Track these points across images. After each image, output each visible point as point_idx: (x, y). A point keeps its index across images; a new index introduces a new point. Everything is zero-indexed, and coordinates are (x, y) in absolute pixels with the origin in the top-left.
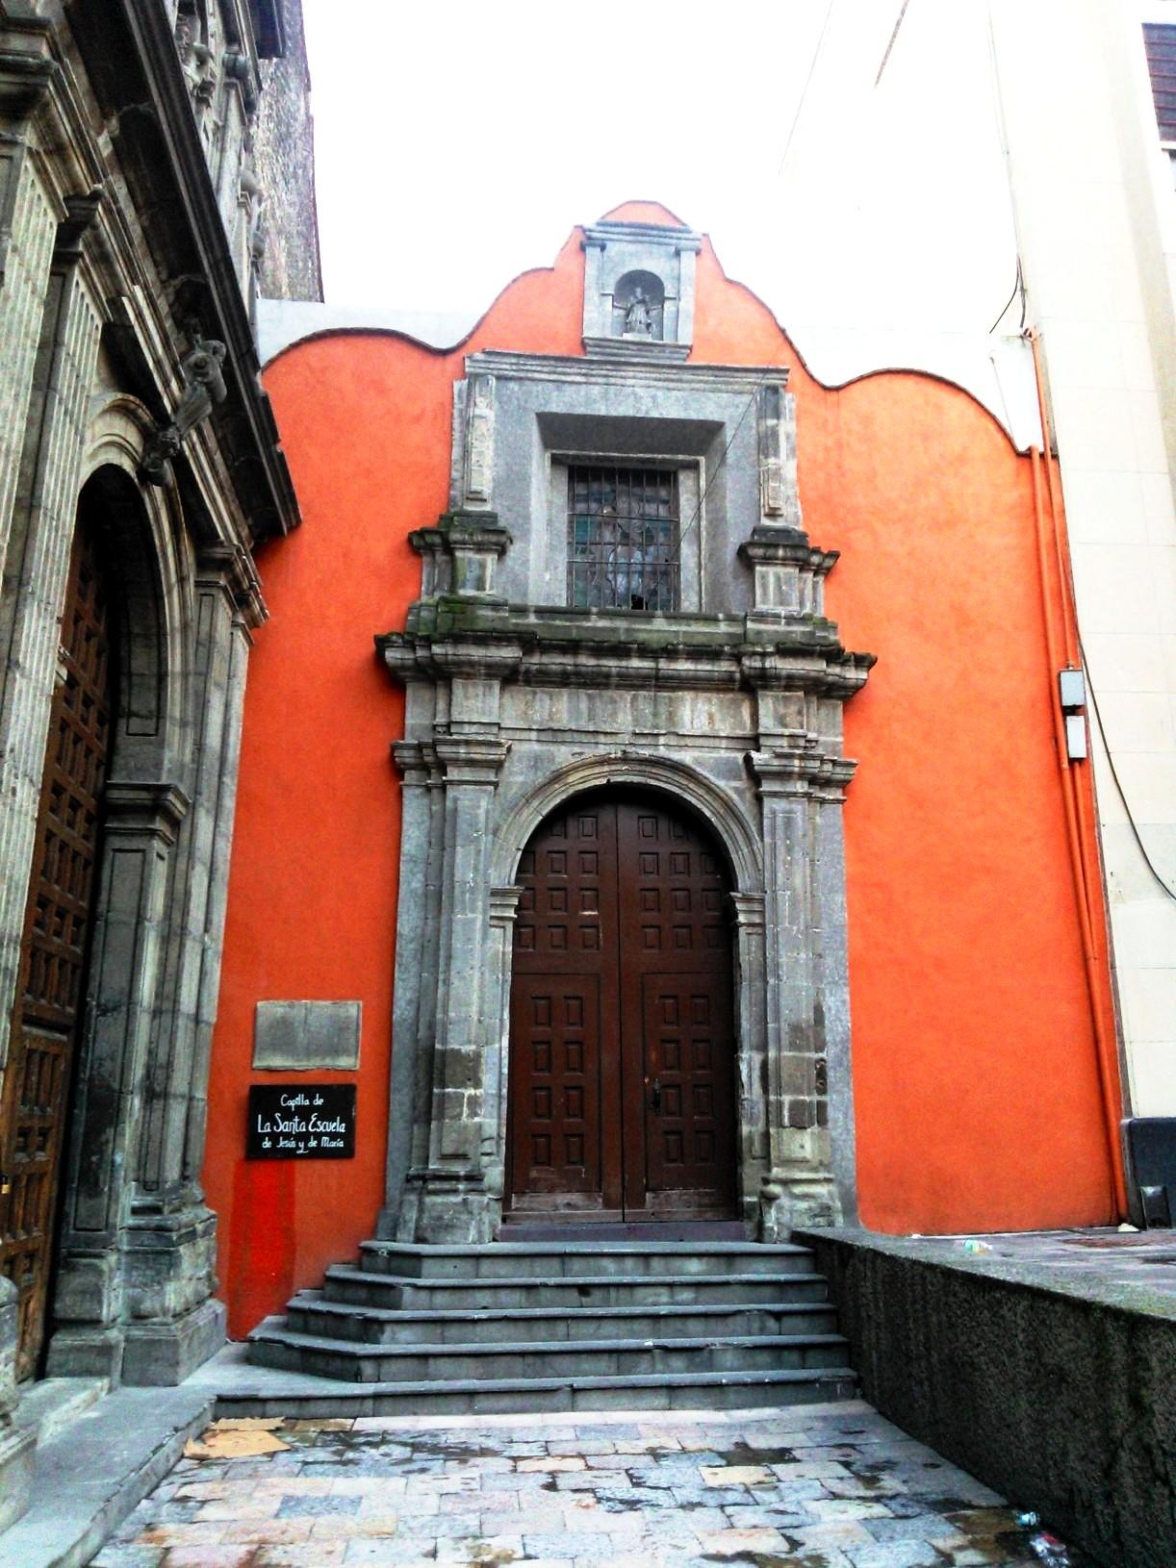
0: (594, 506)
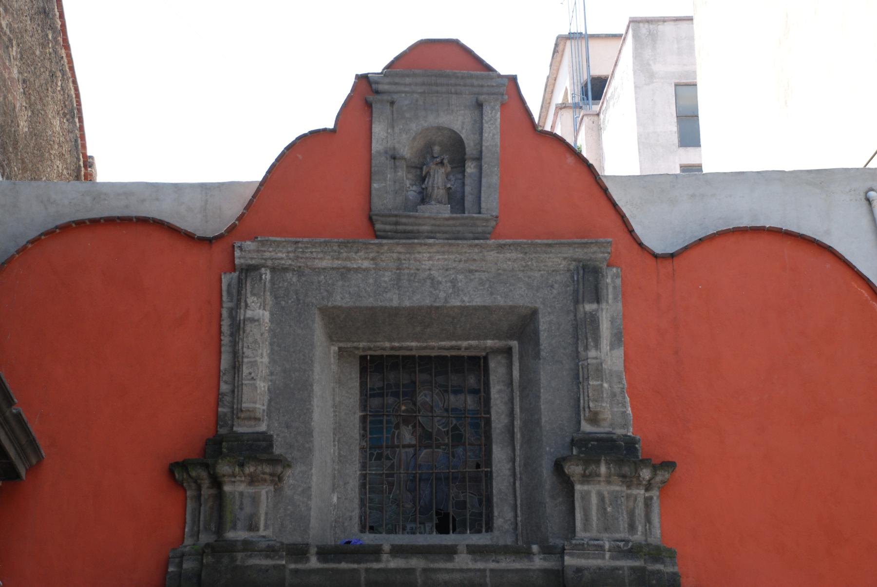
0: (390, 400)
